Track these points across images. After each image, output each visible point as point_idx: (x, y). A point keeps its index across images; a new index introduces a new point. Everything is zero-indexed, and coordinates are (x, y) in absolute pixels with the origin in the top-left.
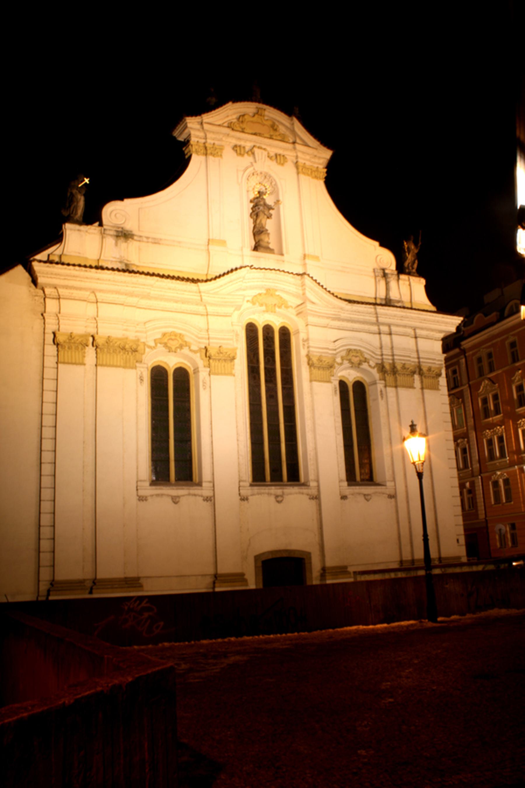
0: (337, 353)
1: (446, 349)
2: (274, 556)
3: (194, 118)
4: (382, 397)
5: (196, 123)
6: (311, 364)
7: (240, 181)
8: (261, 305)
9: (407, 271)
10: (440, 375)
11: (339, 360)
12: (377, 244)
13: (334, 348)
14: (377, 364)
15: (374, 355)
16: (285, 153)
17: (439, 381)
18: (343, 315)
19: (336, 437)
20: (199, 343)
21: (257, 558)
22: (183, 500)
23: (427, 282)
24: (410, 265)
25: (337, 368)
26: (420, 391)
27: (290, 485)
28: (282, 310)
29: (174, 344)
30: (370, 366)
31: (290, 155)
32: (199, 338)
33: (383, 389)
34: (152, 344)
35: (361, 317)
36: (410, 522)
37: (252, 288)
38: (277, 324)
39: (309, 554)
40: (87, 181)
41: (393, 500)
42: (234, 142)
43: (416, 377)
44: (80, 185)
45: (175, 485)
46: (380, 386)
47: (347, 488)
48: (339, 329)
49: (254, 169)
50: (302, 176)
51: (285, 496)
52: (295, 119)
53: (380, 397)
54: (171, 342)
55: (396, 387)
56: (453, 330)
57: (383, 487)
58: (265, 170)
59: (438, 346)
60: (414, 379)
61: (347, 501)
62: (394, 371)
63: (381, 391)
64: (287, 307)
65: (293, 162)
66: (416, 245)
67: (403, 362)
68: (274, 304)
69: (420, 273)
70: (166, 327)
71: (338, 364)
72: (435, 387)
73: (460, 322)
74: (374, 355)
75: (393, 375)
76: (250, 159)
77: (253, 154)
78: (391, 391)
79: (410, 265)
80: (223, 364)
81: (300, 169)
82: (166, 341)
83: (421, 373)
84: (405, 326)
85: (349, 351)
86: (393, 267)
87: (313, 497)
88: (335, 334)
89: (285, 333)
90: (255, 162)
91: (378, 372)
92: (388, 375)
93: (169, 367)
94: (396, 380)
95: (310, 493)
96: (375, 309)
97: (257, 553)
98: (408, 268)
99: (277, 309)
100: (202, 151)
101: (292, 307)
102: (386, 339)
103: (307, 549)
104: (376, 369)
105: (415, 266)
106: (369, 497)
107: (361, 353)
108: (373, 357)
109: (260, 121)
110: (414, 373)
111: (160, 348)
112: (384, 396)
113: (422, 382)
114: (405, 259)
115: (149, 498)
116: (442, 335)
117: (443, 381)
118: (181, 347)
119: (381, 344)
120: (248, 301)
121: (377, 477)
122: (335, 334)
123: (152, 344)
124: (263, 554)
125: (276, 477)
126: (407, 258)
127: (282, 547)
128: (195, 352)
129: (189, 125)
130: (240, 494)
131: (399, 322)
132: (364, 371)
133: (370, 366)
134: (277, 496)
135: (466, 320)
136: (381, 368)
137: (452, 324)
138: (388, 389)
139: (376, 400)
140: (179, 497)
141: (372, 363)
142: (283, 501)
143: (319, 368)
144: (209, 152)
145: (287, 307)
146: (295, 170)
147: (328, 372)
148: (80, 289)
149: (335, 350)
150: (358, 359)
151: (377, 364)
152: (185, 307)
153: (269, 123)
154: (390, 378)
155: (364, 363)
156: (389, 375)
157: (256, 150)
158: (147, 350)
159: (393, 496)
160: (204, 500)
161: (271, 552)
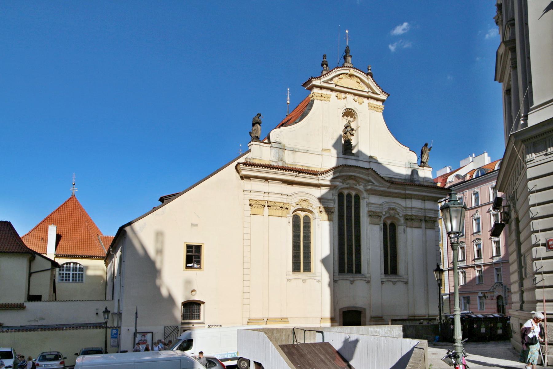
2: (348, 310)
5: (40, 331)
19: (380, 252)
21: (340, 309)
23: (461, 159)
30: (400, 216)
39: (365, 309)
40: (288, 102)
83: (426, 221)
91: (403, 219)
97: (340, 308)
103: (364, 307)
104: (402, 218)
124: (343, 308)
125: (350, 271)
127: (352, 305)
133: (400, 216)
138: (408, 229)
140: (305, 280)
161: (347, 307)
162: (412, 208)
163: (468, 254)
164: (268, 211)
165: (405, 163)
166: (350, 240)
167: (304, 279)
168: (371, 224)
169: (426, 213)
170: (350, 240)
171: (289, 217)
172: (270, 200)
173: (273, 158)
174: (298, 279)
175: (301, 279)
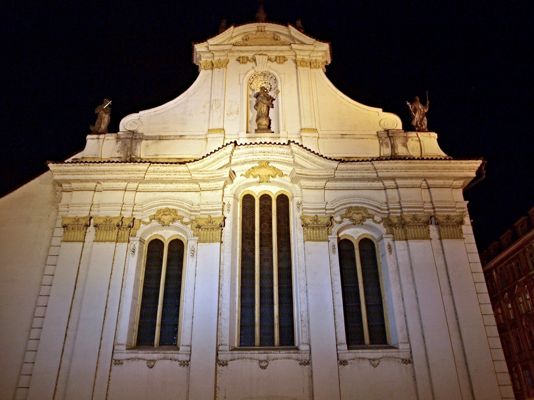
0: (336, 212)
1: (467, 194)
3: (201, 44)
4: (390, 252)
6: (305, 225)
7: (241, 82)
8: (255, 177)
9: (417, 129)
10: (462, 223)
11: (338, 219)
12: (380, 110)
13: (333, 208)
14: (383, 219)
15: (379, 210)
16: (285, 54)
17: (461, 230)
18: (338, 174)
20: (191, 215)
22: (158, 364)
24: (418, 123)
25: (335, 227)
26: (439, 241)
27: (283, 349)
28: (277, 179)
29: (166, 219)
31: (289, 55)
32: (191, 211)
33: (391, 243)
34: (147, 220)
35: (358, 174)
36: (433, 394)
37: (245, 162)
38: (274, 191)
41: (409, 365)
42: (237, 55)
43: (432, 228)
44: (104, 108)
45: (158, 349)
46: (387, 240)
47: (347, 351)
48: (336, 189)
49: (255, 71)
50: (300, 68)
51: (271, 362)
52: (290, 26)
53: (387, 251)
54: (164, 217)
55: (406, 240)
56: (473, 174)
57: (394, 350)
58: (265, 69)
59: (459, 195)
60: (429, 230)
61: (347, 367)
62: (403, 224)
63: (389, 245)
64: (282, 175)
65: (293, 60)
66: (424, 104)
67: (414, 213)
68: (268, 174)
69: (430, 129)
70: (161, 205)
71: (336, 222)
72: (459, 236)
73: (479, 165)
74: (379, 210)
75: (403, 228)
76: (253, 64)
77: (255, 60)
78: (400, 245)
79: (418, 123)
80: (211, 232)
81: (298, 64)
82: (160, 216)
84: (411, 178)
85: (350, 209)
86: (400, 126)
87: (305, 362)
88: (330, 195)
89: (283, 200)
90: (256, 65)
92: (396, 228)
93: (165, 239)
94: (406, 233)
95: (300, 358)
96: (373, 164)
98: (417, 126)
99: (271, 179)
100: (210, 67)
101: (286, 175)
102: (392, 193)
105: (426, 122)
106: (377, 362)
107: (365, 209)
108: (379, 212)
109: (263, 36)
110: (427, 223)
111: (155, 223)
112: (393, 251)
113: (439, 232)
114: (412, 118)
115: (125, 362)
116: (460, 183)
117: (468, 228)
118: (174, 220)
119: (387, 199)
120: (242, 175)
121: (391, 339)
122: (330, 195)
123: (147, 220)
126: (415, 117)
128: (186, 224)
129: (198, 50)
130: (338, 359)
131: (403, 174)
132: (369, 227)
133: (375, 221)
134: (260, 361)
135: (486, 162)
136: (388, 223)
137: (470, 169)
138: (397, 243)
139: (384, 255)
140: (154, 361)
141: (378, 218)
142: (155, 367)
143: (313, 228)
144: (215, 65)
145: (282, 175)
146: (294, 65)
147: (325, 231)
148: (87, 181)
149: (333, 209)
150: (360, 215)
151: (383, 219)
152: (180, 186)
153: (271, 36)
154: (398, 231)
155: (367, 220)
156: (398, 228)
157: (257, 57)
158: (142, 225)
159: (408, 361)
160: (181, 365)
162: (145, 174)
163: (219, 210)
164: (94, 233)
165: (377, 132)
166: (267, 276)
167: (150, 360)
168: (308, 240)
169: (436, 209)
170: (267, 276)
171: (135, 243)
172: (498, 384)
173: (117, 154)
174: (139, 359)
175: (144, 360)
